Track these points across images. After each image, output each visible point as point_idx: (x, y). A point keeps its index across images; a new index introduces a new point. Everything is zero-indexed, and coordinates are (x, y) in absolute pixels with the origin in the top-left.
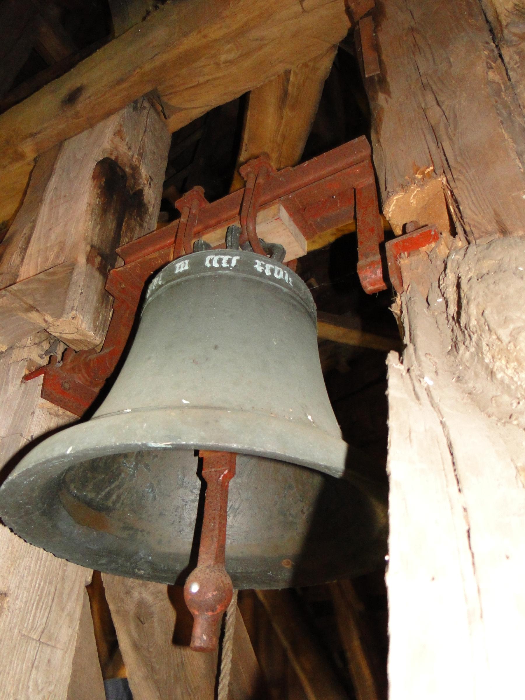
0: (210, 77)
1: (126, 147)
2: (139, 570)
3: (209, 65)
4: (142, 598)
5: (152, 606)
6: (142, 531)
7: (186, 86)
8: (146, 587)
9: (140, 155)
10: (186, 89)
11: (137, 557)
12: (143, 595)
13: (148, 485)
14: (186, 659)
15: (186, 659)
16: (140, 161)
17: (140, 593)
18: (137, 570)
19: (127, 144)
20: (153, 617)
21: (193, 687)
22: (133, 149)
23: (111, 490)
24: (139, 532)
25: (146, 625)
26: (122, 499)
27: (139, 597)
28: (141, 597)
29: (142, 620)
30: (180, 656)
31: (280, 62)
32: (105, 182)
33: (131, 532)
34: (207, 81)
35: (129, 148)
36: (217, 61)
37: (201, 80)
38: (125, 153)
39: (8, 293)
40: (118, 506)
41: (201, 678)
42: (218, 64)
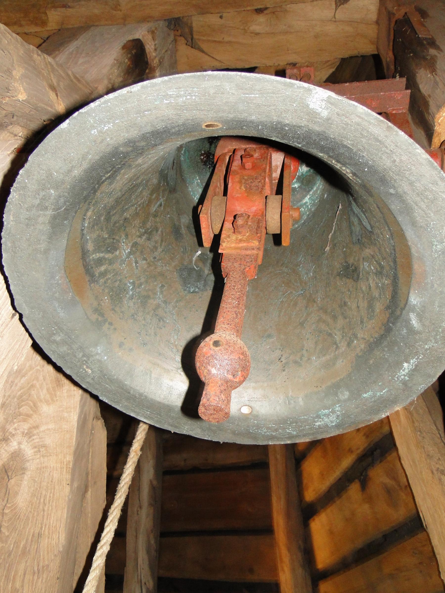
0: (233, 40)
1: (153, 47)
2: (87, 367)
3: (238, 28)
4: (20, 449)
5: (28, 461)
6: (111, 324)
7: (210, 38)
8: (30, 437)
9: (160, 62)
10: (209, 41)
11: (93, 350)
12: (22, 447)
13: (131, 281)
14: (47, 531)
15: (47, 531)
16: (158, 66)
17: (20, 443)
18: (85, 367)
19: (155, 45)
20: (24, 473)
21: (41, 564)
22: (157, 52)
23: (104, 258)
24: (107, 323)
25: (12, 481)
26: (107, 277)
27: (17, 447)
28: (19, 447)
29: (10, 474)
30: (40, 526)
31: (295, 53)
32: (135, 53)
33: (100, 319)
34: (229, 42)
35: (155, 50)
36: (246, 28)
37: (227, 39)
38: (150, 52)
39: (42, 57)
40: (102, 281)
41: (55, 556)
42: (245, 31)
